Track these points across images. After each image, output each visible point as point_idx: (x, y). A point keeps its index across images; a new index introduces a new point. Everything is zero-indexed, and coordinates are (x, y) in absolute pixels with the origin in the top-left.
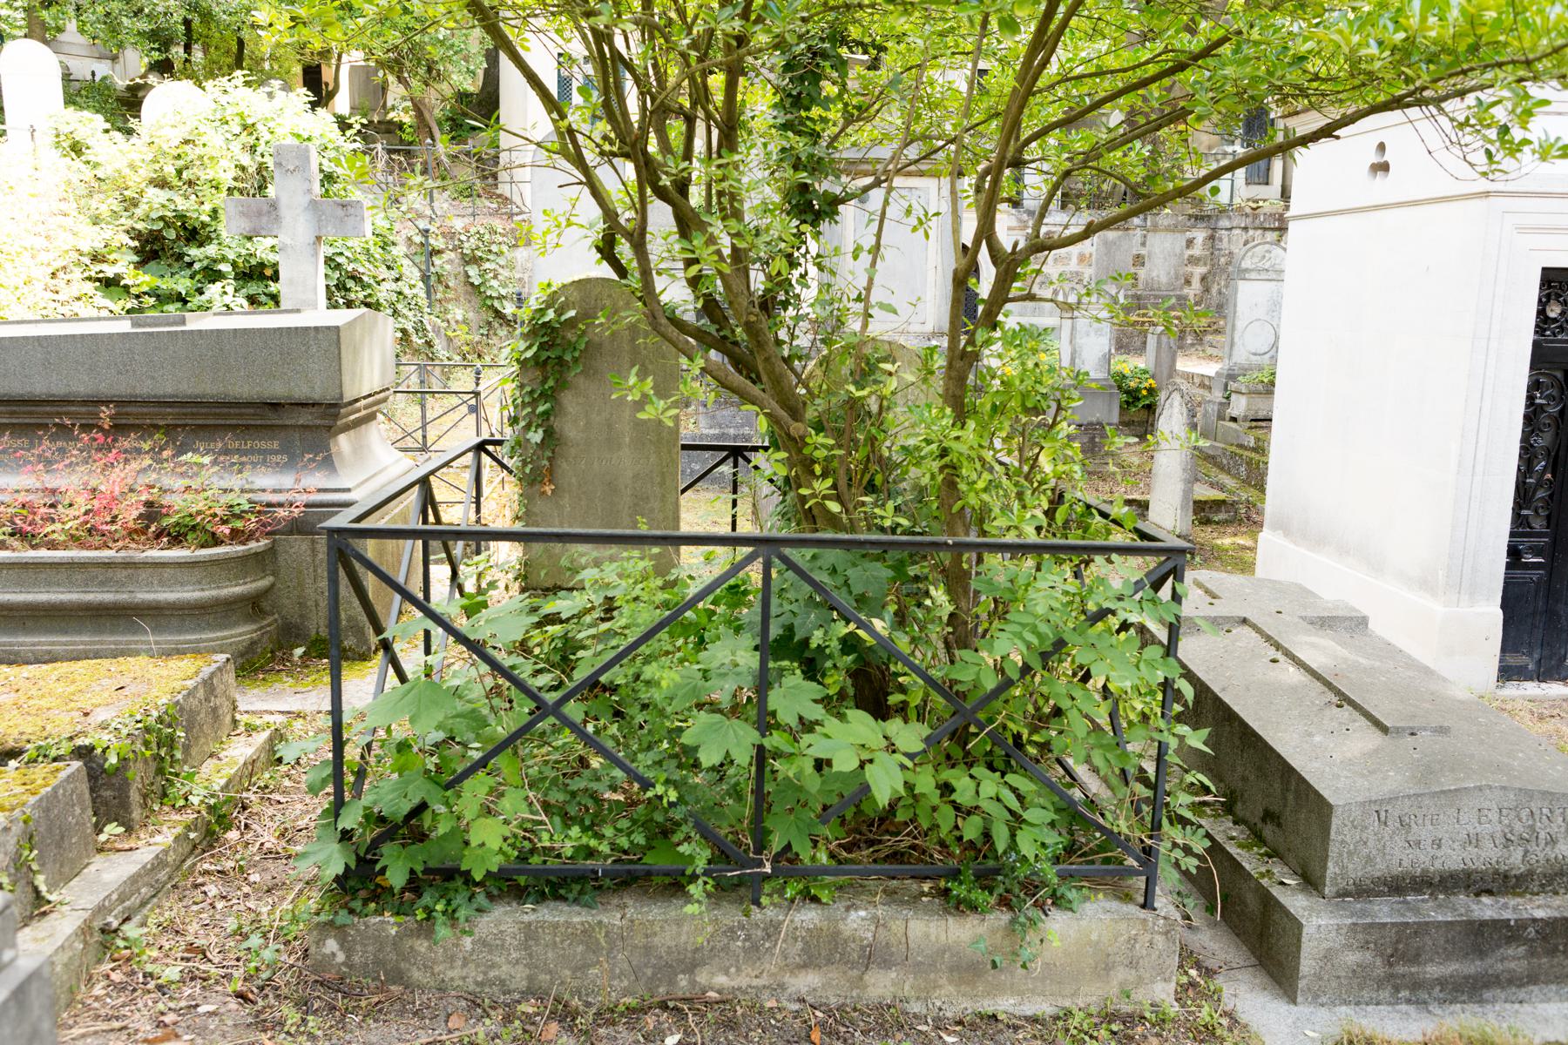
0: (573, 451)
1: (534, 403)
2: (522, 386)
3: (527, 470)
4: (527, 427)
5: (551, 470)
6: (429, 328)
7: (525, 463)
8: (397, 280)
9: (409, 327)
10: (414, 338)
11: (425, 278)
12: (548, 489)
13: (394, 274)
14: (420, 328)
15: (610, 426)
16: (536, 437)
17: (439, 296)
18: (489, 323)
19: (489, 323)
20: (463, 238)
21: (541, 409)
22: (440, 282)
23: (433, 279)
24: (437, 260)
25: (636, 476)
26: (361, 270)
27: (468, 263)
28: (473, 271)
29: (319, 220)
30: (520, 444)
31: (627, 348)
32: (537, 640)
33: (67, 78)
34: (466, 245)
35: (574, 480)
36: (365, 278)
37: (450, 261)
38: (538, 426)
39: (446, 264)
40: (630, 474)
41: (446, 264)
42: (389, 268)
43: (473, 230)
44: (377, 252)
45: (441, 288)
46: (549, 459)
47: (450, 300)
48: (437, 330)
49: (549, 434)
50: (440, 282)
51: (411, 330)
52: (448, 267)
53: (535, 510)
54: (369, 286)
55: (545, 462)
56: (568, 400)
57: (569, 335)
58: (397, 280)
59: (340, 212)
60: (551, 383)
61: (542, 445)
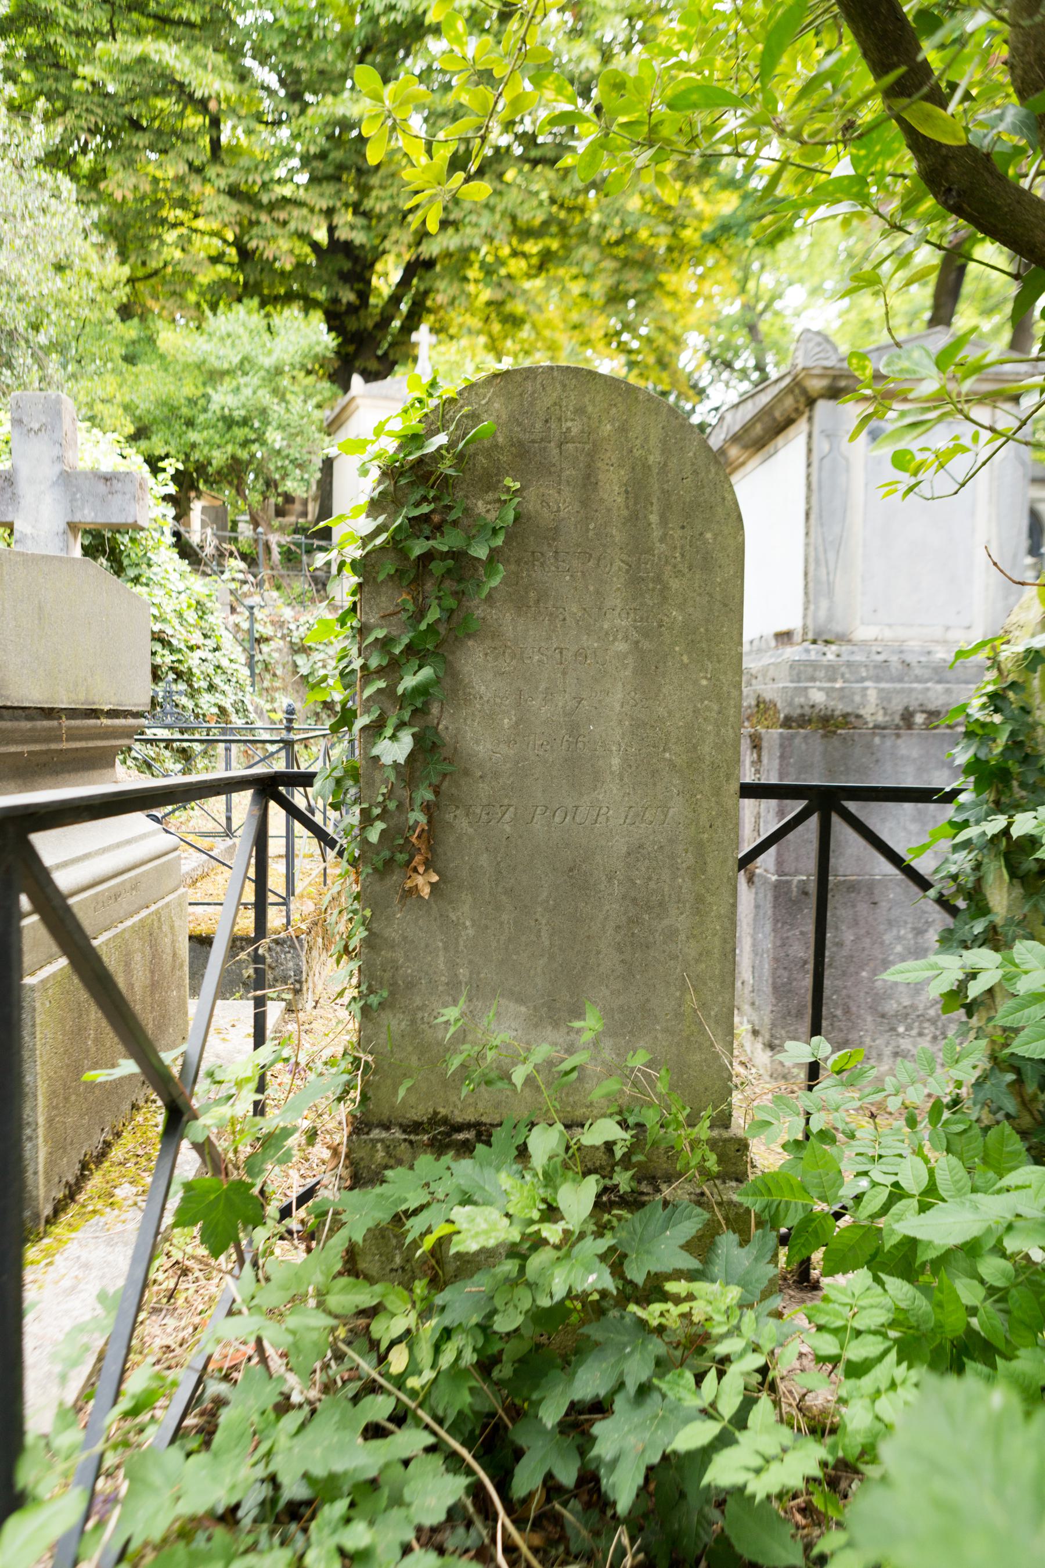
0: (484, 789)
1: (392, 668)
2: (362, 631)
3: (374, 836)
4: (375, 730)
5: (432, 834)
6: (251, 708)
7: (367, 819)
8: (215, 650)
9: (227, 704)
10: (234, 718)
11: (251, 664)
12: (423, 882)
13: (211, 643)
14: (241, 709)
15: (574, 729)
16: (395, 750)
17: (266, 684)
18: (317, 714)
19: (317, 714)
20: (293, 627)
21: (409, 682)
22: (267, 669)
23: (260, 666)
24: (265, 648)
25: (635, 852)
26: (170, 631)
27: (296, 652)
28: (300, 660)
29: (73, 500)
30: (355, 775)
31: (618, 534)
32: (398, 1326)
33: (614, 1143)
34: (295, 634)
35: (484, 860)
36: (174, 642)
37: (279, 650)
38: (401, 725)
39: (273, 651)
40: (620, 845)
41: (273, 651)
42: (205, 636)
43: (302, 620)
44: (191, 616)
45: (268, 676)
46: (428, 808)
47: (277, 689)
48: (260, 713)
49: (427, 747)
50: (267, 669)
51: (230, 710)
52: (276, 655)
53: (392, 933)
54: (180, 651)
55: (418, 817)
56: (475, 662)
57: (481, 507)
58: (215, 650)
59: (102, 488)
60: (433, 615)
61: (410, 771)
